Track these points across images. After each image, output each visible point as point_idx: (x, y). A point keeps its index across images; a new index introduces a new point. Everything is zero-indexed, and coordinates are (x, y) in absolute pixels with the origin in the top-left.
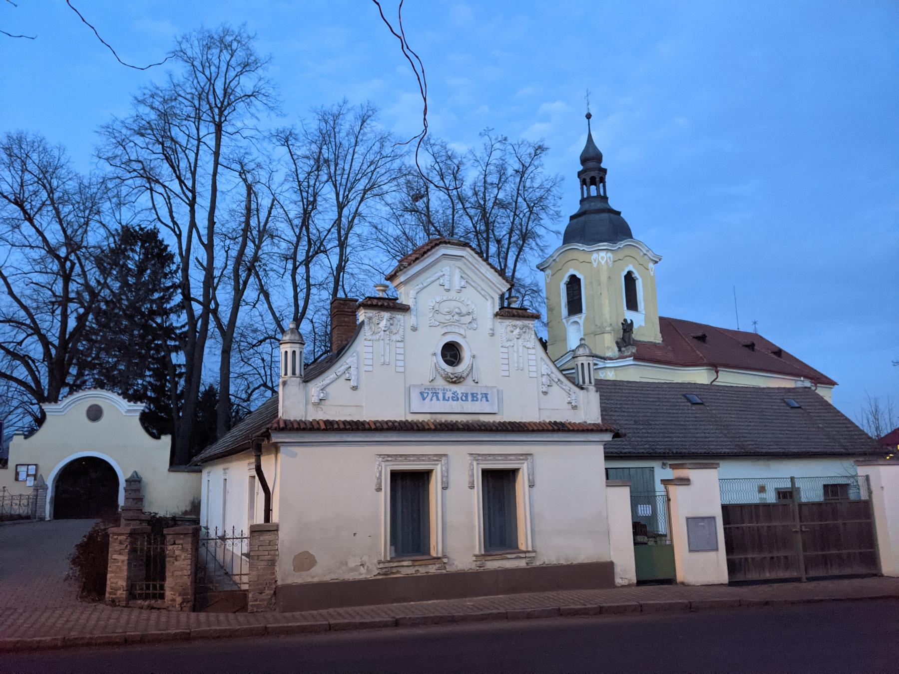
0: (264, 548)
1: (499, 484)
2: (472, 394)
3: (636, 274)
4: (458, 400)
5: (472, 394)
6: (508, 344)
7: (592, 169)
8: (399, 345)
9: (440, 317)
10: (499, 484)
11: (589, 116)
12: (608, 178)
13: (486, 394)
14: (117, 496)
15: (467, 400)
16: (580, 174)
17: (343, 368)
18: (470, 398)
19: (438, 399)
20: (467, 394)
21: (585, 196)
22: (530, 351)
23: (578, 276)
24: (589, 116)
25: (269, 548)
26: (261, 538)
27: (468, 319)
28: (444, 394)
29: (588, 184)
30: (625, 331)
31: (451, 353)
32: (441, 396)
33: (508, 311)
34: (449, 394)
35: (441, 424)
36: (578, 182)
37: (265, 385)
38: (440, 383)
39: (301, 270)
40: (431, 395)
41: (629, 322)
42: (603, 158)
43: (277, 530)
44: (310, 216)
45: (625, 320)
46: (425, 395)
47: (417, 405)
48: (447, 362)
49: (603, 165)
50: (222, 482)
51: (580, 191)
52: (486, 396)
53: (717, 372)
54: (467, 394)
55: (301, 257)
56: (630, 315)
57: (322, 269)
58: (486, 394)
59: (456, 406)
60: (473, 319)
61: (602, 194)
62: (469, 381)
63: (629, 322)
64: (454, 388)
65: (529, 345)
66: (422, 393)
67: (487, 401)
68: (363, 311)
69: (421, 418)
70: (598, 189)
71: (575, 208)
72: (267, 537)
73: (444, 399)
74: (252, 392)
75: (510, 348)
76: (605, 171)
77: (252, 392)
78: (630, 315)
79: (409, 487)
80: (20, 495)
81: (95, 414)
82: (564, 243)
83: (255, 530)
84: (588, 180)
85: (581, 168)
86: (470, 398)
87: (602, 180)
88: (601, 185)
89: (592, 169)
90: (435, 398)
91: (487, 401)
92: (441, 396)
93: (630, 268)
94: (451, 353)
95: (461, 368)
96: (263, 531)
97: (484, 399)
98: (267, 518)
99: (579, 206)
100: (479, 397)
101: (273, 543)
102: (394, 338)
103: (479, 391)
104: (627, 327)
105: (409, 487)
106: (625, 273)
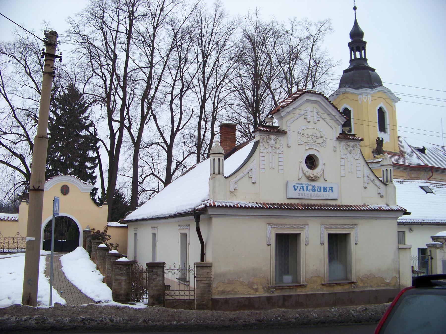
0: (204, 276)
1: (338, 243)
2: (324, 187)
3: (385, 109)
4: (315, 191)
5: (324, 187)
6: (344, 157)
7: (357, 41)
8: (280, 156)
9: (304, 139)
10: (338, 243)
11: (355, 8)
12: (367, 47)
13: (332, 188)
14: (40, 241)
15: (320, 191)
16: (350, 44)
17: (247, 170)
18: (322, 189)
19: (303, 190)
20: (321, 187)
21: (353, 58)
22: (358, 161)
23: (349, 108)
24: (355, 8)
25: (207, 276)
26: (202, 271)
27: (320, 141)
28: (307, 187)
29: (355, 50)
30: (378, 144)
31: (311, 161)
32: (305, 188)
33: (346, 136)
34: (310, 187)
35: (308, 205)
36: (348, 49)
37: (153, 174)
38: (305, 181)
39: (177, 101)
40: (299, 188)
41: (381, 139)
42: (364, 35)
43: (211, 266)
44: (254, 82)
45: (378, 138)
46: (296, 188)
47: (293, 194)
48: (308, 166)
49: (364, 39)
50: (150, 237)
51: (349, 55)
52: (331, 188)
53: (432, 172)
54: (321, 187)
55: (177, 92)
56: (381, 135)
57: (192, 101)
58: (332, 188)
59: (314, 195)
60: (324, 140)
61: (353, 53)
62: (321, 179)
63: (381, 139)
64: (313, 183)
65: (356, 157)
66: (294, 187)
67: (332, 191)
68: (259, 134)
69: (293, 202)
70: (361, 55)
71: (347, 65)
72: (205, 270)
73: (307, 190)
74: (145, 178)
75: (346, 159)
76: (365, 43)
77: (145, 178)
78: (381, 135)
79: (287, 243)
80: (9, 238)
81: (65, 190)
82: (340, 87)
83: (198, 266)
84: (355, 48)
85: (350, 40)
86: (322, 189)
87: (364, 49)
88: (363, 51)
89: (357, 41)
90: (302, 190)
91: (332, 191)
92: (305, 188)
93: (381, 105)
94: (311, 161)
95: (317, 172)
96: (203, 266)
97: (330, 191)
98: (202, 259)
99: (349, 64)
100: (328, 189)
101: (209, 274)
102: (278, 151)
103: (328, 185)
104: (380, 142)
105: (287, 243)
106: (378, 108)
